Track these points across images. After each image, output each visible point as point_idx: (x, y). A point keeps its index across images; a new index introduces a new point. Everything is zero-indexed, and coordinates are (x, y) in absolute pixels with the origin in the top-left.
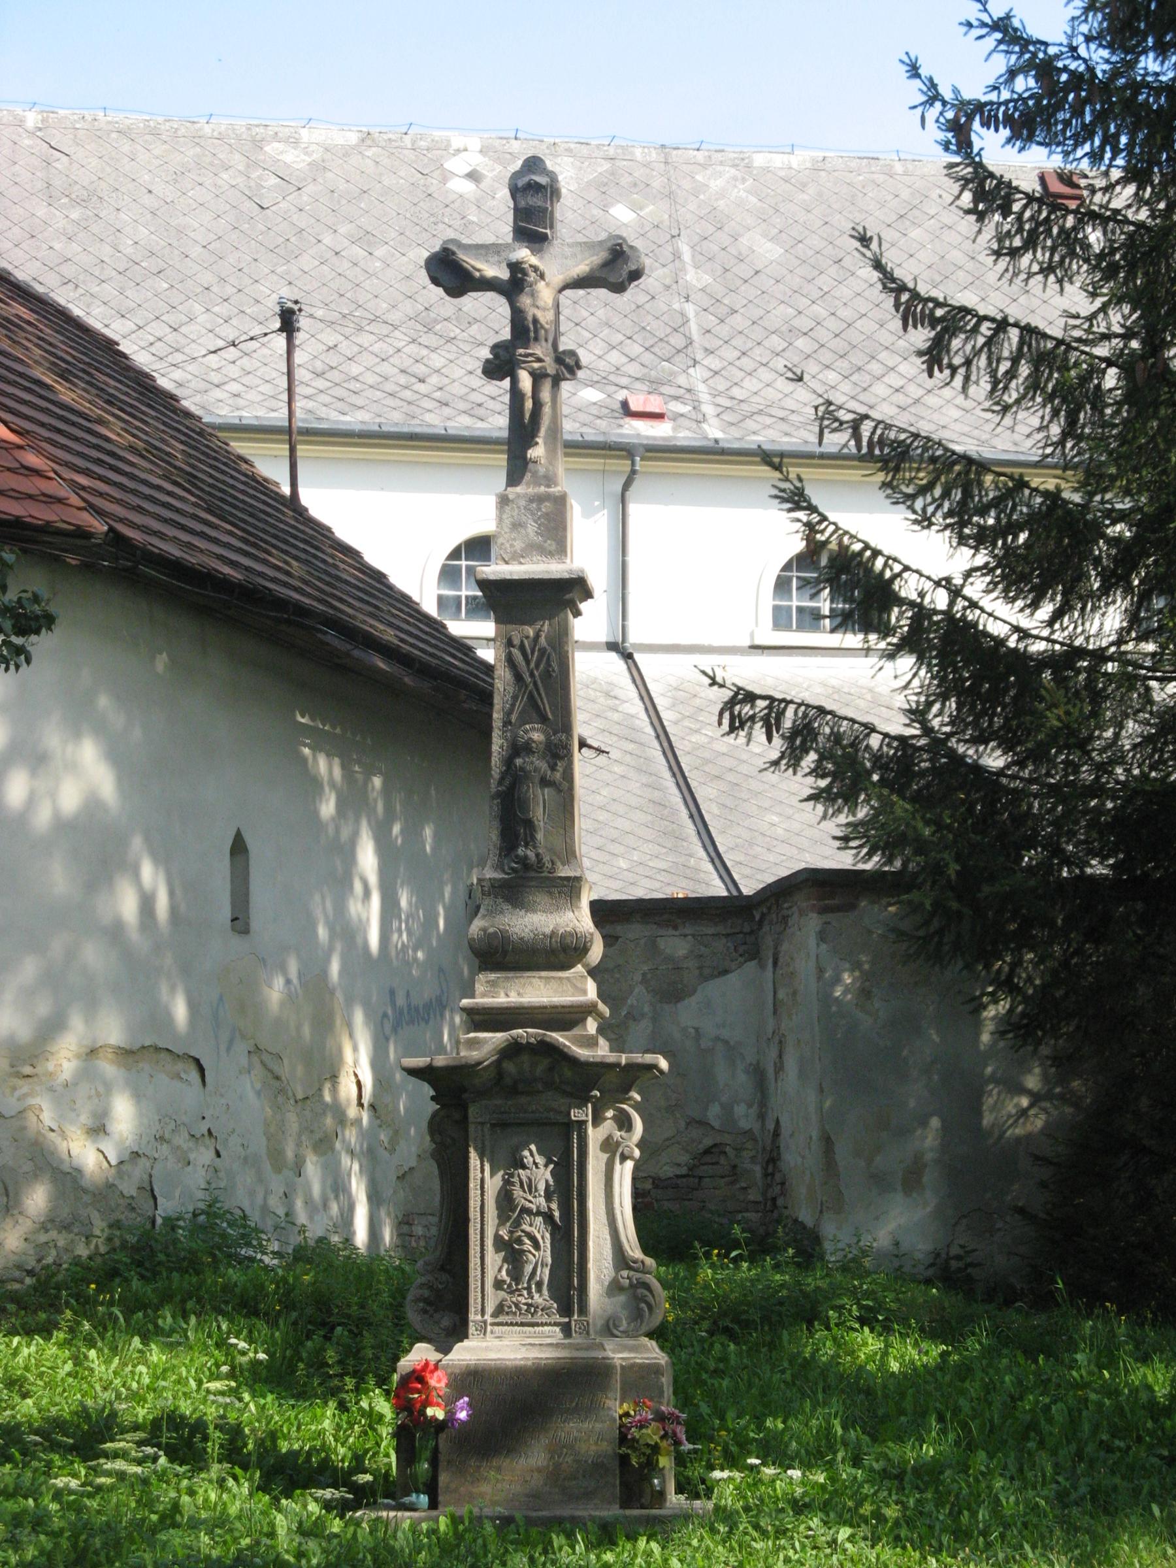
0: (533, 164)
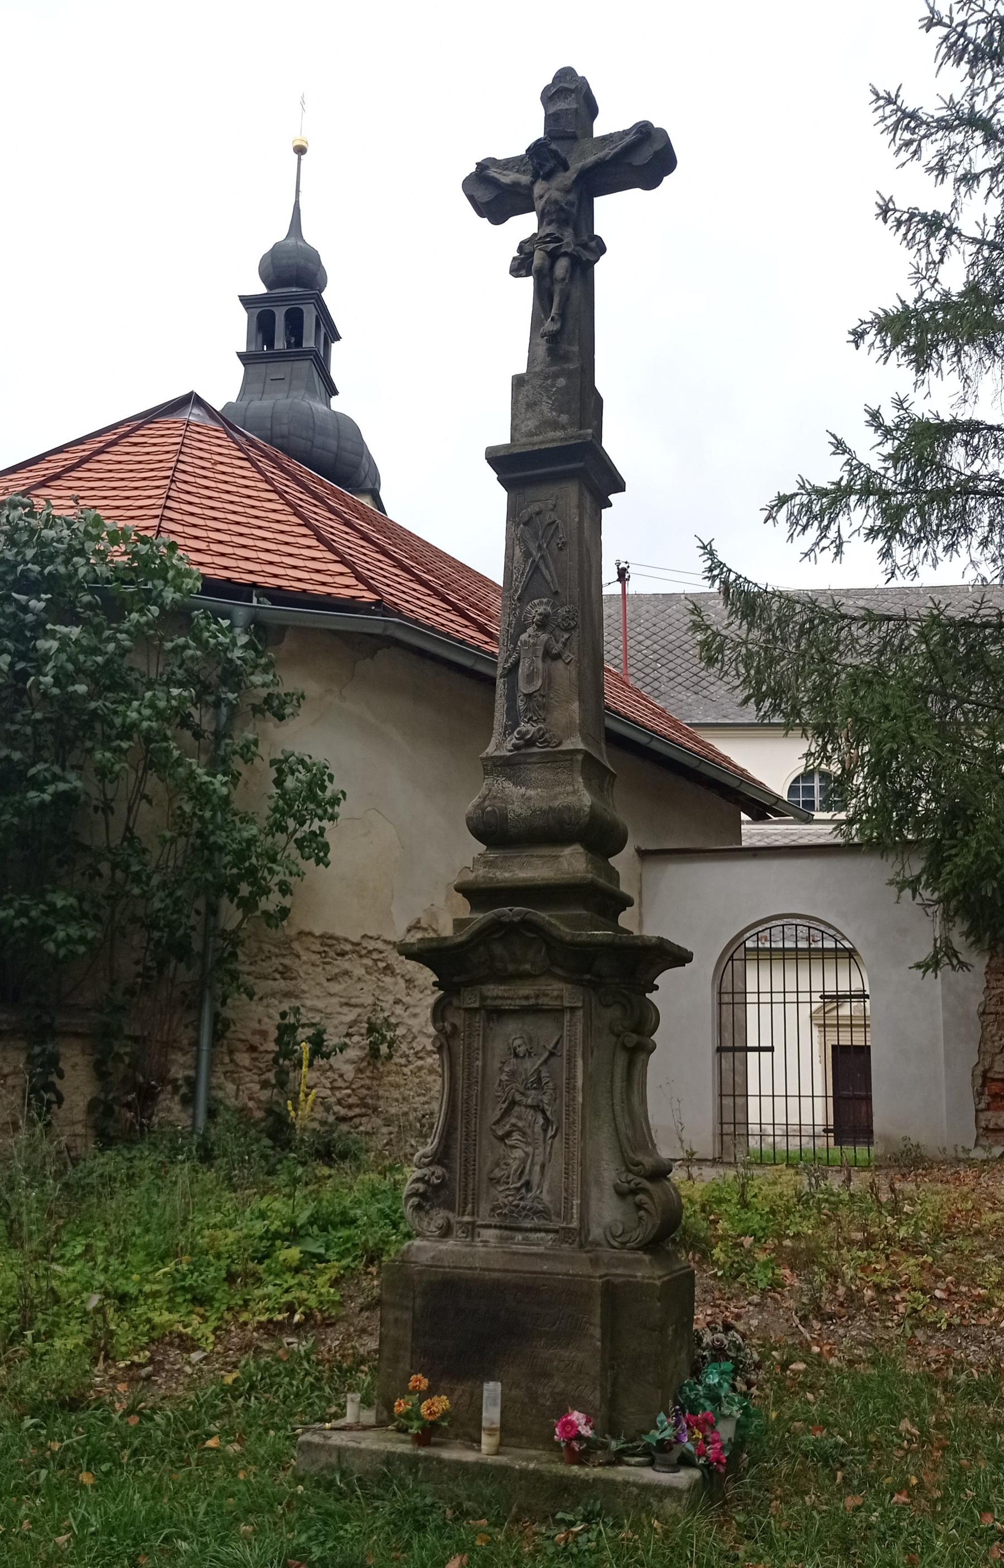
0: (566, 75)
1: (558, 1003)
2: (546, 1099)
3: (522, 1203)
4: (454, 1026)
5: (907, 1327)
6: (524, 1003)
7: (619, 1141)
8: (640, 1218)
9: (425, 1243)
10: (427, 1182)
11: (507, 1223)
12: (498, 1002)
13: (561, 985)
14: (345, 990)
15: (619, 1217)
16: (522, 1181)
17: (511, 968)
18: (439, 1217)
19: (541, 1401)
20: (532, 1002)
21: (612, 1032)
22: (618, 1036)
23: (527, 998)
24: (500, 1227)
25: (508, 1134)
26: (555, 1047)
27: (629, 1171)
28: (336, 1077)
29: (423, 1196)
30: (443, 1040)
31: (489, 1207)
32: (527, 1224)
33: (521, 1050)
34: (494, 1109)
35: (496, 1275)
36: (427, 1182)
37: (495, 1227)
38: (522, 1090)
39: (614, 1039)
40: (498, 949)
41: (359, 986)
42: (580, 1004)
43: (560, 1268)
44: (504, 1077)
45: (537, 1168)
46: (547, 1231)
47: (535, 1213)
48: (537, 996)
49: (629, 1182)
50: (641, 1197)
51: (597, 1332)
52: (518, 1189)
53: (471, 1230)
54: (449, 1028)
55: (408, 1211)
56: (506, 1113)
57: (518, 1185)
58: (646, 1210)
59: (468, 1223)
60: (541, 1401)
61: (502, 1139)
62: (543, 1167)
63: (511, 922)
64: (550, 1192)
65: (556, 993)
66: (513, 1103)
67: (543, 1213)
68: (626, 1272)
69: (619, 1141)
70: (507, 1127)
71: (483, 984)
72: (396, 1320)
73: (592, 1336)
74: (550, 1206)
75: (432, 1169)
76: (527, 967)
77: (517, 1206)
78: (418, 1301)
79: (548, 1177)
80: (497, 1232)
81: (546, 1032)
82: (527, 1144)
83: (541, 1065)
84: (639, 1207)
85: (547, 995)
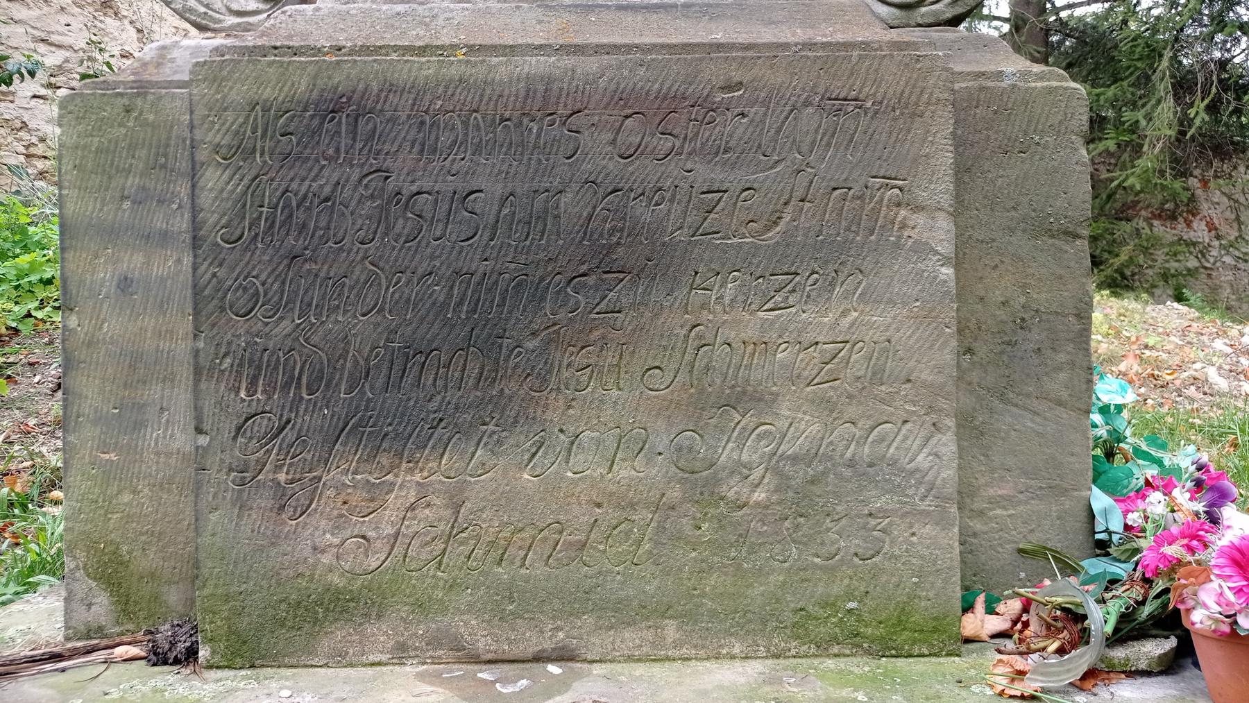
14: (38, 18)
28: (34, 140)
35: (534, 64)
41: (64, 19)
51: (939, 232)
60: (732, 489)
72: (125, 284)
73: (922, 249)
78: (212, 178)
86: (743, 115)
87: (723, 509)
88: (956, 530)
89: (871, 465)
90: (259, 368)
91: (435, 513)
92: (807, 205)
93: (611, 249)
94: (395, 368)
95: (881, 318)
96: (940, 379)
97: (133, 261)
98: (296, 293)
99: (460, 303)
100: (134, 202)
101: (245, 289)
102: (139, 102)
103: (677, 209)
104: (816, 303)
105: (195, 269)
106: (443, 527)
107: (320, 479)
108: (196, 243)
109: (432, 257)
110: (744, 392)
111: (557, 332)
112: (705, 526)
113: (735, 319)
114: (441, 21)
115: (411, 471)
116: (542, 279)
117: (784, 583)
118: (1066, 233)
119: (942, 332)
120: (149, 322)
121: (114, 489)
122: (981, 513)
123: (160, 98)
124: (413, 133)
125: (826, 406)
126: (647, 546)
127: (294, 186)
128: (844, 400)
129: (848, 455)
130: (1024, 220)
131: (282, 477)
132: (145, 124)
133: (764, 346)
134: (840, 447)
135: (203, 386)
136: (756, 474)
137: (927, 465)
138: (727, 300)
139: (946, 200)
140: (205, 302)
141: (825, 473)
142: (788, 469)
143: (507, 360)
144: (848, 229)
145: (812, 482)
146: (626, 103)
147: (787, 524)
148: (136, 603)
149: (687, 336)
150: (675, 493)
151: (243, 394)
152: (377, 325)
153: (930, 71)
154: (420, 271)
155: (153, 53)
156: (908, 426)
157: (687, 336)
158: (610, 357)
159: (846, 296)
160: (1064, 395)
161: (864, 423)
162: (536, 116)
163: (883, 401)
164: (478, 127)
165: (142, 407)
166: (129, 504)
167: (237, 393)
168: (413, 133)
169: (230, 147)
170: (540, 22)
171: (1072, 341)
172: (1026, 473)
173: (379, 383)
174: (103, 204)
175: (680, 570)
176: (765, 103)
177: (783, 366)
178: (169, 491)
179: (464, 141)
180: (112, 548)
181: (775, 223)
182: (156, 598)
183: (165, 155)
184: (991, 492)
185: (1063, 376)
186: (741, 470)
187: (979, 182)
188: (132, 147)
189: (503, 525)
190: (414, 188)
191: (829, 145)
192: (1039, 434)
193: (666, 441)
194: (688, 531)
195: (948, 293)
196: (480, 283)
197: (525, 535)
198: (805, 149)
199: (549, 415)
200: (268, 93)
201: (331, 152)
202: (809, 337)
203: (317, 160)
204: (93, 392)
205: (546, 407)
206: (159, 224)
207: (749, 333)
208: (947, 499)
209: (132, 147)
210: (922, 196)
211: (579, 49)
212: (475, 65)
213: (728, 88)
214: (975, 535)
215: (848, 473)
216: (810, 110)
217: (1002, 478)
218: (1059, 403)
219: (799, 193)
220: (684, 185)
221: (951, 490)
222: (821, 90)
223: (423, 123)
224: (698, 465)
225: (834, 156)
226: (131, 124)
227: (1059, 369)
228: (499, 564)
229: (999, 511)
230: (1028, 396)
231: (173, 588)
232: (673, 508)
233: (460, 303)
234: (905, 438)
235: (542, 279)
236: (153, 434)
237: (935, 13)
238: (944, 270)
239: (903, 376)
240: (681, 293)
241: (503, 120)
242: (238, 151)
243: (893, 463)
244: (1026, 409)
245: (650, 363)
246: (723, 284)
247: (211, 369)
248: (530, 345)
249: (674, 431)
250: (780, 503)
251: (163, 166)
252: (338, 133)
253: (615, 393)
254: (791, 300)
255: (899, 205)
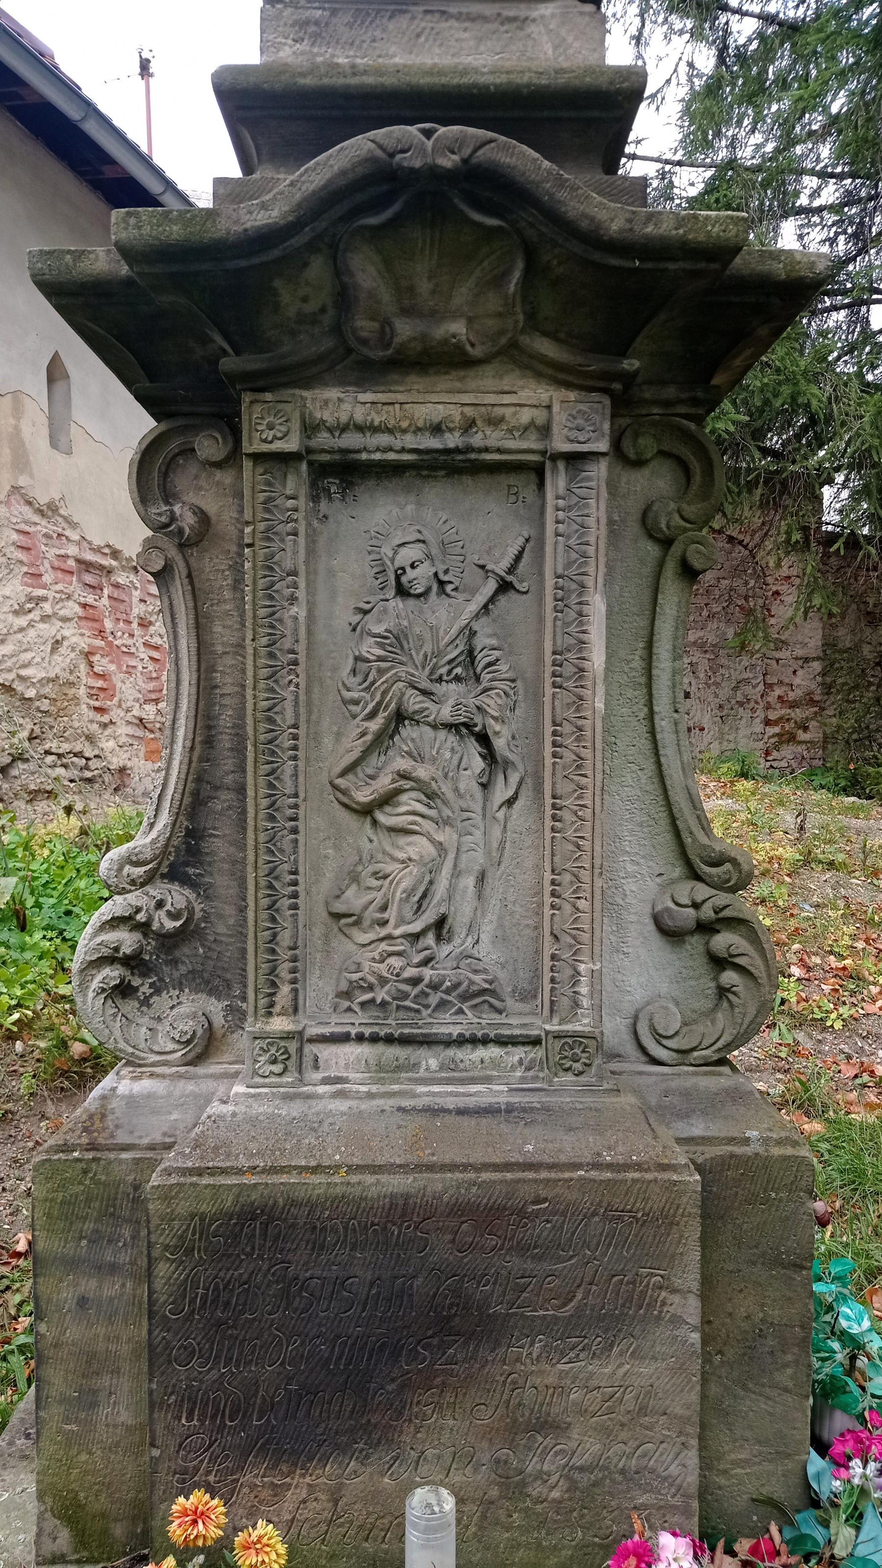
1: (531, 443)
2: (493, 703)
3: (428, 973)
4: (204, 518)
5: (784, 1030)
6: (434, 443)
7: (668, 804)
8: (723, 992)
9: (146, 1085)
10: (144, 928)
11: (392, 1025)
12: (351, 440)
13: (543, 393)
15: (664, 988)
16: (429, 916)
17: (405, 330)
18: (184, 1011)
19: (536, 1490)
20: (452, 440)
21: (651, 535)
22: (666, 543)
23: (437, 429)
24: (374, 1039)
25: (388, 800)
26: (511, 570)
27: (696, 876)
29: (133, 962)
30: (173, 552)
31: (330, 990)
32: (448, 1025)
33: (420, 577)
34: (338, 735)
36: (144, 928)
37: (360, 1038)
38: (425, 684)
39: (652, 550)
40: (366, 272)
42: (603, 446)
43: (571, 1145)
44: (370, 649)
45: (469, 882)
46: (503, 1042)
47: (465, 997)
48: (469, 425)
49: (696, 906)
50: (723, 941)
51: (690, 1309)
52: (415, 937)
53: (291, 1054)
54: (188, 521)
55: (91, 1002)
56: (381, 742)
57: (416, 927)
58: (742, 970)
59: (288, 1036)
61: (366, 811)
62: (482, 878)
63: (434, 173)
64: (501, 939)
65: (525, 416)
66: (400, 717)
67: (484, 996)
68: (716, 1129)
69: (668, 804)
70: (384, 783)
71: (307, 383)
72: (82, 1302)
73: (677, 1320)
74: (502, 975)
75: (156, 891)
76: (458, 328)
77: (415, 981)
78: (163, 1269)
79: (494, 902)
80: (364, 1050)
81: (485, 527)
82: (442, 822)
83: (477, 616)
84: (719, 963)
85: (495, 422)
86: (548, 1221)
87: (528, 1503)
88: (696, 1519)
89: (637, 1473)
90: (195, 1403)
91: (321, 1505)
92: (594, 1288)
93: (450, 1318)
94: (293, 1404)
95: (646, 1369)
96: (688, 1413)
97: (89, 1285)
98: (222, 1350)
99: (339, 1358)
100: (89, 1241)
101: (186, 1348)
102: (94, 1166)
103: (499, 1289)
104: (600, 1358)
105: (150, 1332)
106: (327, 1515)
107: (237, 1480)
108: (151, 1315)
109: (320, 1325)
110: (546, 1422)
111: (410, 1379)
112: (515, 1516)
113: (542, 1371)
114: (325, 1127)
115: (303, 1476)
116: (399, 1340)
117: (572, 1557)
118: (795, 1265)
119: (690, 1381)
120: (101, 1330)
121: (75, 1452)
122: (725, 1472)
123: (110, 1163)
124: (308, 1235)
125: (605, 1432)
126: (473, 1529)
127: (222, 1274)
128: (618, 1427)
129: (621, 1465)
130: (763, 1254)
131: (211, 1478)
132: (98, 1183)
133: (560, 1390)
134: (615, 1460)
135: (156, 1416)
136: (554, 1479)
137: (676, 1473)
138: (535, 1355)
139: (695, 1286)
140: (156, 1357)
141: (604, 1478)
142: (577, 1476)
143: (373, 1399)
144: (623, 1305)
145: (593, 1485)
146: (460, 1210)
147: (575, 1514)
148: (90, 1536)
149: (504, 1382)
150: (494, 1492)
151: (183, 1421)
152: (279, 1374)
153: (685, 1192)
154: (311, 1335)
155: (96, 1104)
156: (664, 1445)
157: (504, 1382)
158: (449, 1397)
159: (621, 1354)
160: (790, 1384)
161: (633, 1444)
162: (397, 1224)
163: (647, 1428)
164: (354, 1230)
165: (95, 1392)
166: (86, 1462)
167: (180, 1420)
168: (308, 1235)
169: (176, 1247)
170: (399, 1127)
171: (798, 1345)
172: (759, 1442)
173: (281, 1415)
174: (66, 1242)
175: (497, 1546)
176: (564, 1214)
177: (575, 1404)
178: (116, 1453)
179: (345, 1241)
180: (70, 1496)
181: (571, 1300)
182: (105, 1532)
183: (114, 1206)
184: (733, 1456)
185: (789, 1371)
186: (541, 1476)
187: (729, 1226)
188: (88, 1200)
189: (369, 1514)
190: (308, 1275)
191: (610, 1244)
192: (770, 1414)
193: (488, 1456)
194: (503, 1518)
195: (695, 1352)
196: (354, 1344)
197: (386, 1521)
198: (593, 1247)
199: (403, 1438)
200: (203, 1208)
201: (248, 1249)
202: (594, 1383)
203: (238, 1256)
204: (58, 1380)
205: (401, 1432)
206: (109, 1258)
207: (551, 1380)
208: (689, 1497)
209: (88, 1200)
210: (677, 1282)
211: (430, 1168)
212: (353, 1185)
213: (535, 1203)
214: (720, 1488)
215: (619, 1478)
216: (597, 1219)
217: (742, 1446)
218: (786, 1390)
219: (587, 1279)
220: (504, 1272)
221: (694, 1490)
222: (605, 1204)
223: (315, 1227)
224: (511, 1473)
225: (613, 1253)
226: (87, 1182)
227: (786, 1366)
228: (366, 1540)
229: (739, 1471)
230: (763, 1385)
231: (119, 1525)
232: (492, 1503)
233: (339, 1358)
234: (662, 1454)
235: (399, 1340)
236: (104, 1412)
237: (704, 1057)
238: (693, 1335)
239: (661, 1411)
240: (501, 1351)
241: (373, 1224)
242: (183, 1249)
243: (652, 1471)
244: (761, 1395)
245: (478, 1401)
246: (532, 1344)
247: (162, 1403)
248: (390, 1388)
249: (494, 1449)
250: (570, 1499)
251: (112, 1214)
252: (254, 1235)
253: (451, 1422)
254: (582, 1356)
255: (661, 1288)
